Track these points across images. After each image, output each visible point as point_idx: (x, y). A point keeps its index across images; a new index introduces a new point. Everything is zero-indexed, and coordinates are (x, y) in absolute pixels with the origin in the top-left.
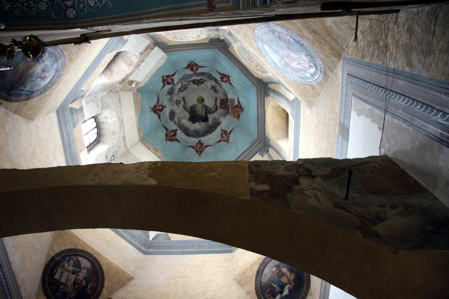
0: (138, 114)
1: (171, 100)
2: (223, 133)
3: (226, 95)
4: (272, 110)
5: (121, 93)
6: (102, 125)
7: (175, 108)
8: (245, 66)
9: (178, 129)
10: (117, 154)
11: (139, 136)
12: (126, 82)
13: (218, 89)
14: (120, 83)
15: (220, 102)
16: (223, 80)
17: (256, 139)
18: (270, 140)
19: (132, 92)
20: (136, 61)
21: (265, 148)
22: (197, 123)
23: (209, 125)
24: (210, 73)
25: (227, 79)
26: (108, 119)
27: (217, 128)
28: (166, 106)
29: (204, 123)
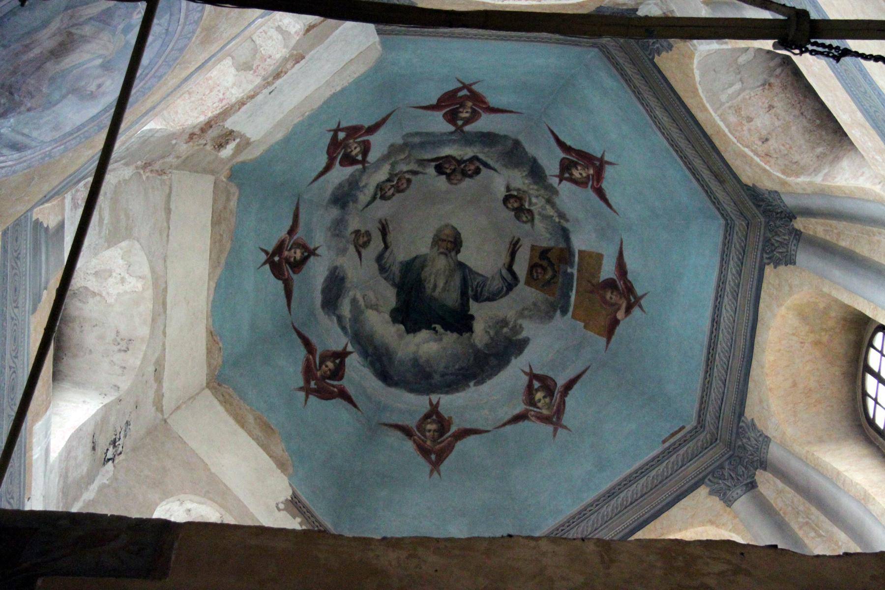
0: (219, 271)
1: (337, 228)
2: (536, 384)
3: (565, 234)
4: (793, 320)
5: (176, 175)
6: (79, 304)
7: (349, 264)
8: (709, 131)
9: (350, 348)
10: (125, 436)
11: (209, 365)
12: (212, 133)
13: (532, 208)
14: (192, 136)
15: (531, 258)
16: (567, 175)
17: (688, 428)
18: (767, 440)
19: (211, 178)
20: (278, 56)
21: (734, 470)
22: (424, 334)
23: (473, 346)
24: (521, 138)
25: (591, 172)
26: (111, 281)
27: (507, 362)
28: (317, 252)
29: (455, 335)
